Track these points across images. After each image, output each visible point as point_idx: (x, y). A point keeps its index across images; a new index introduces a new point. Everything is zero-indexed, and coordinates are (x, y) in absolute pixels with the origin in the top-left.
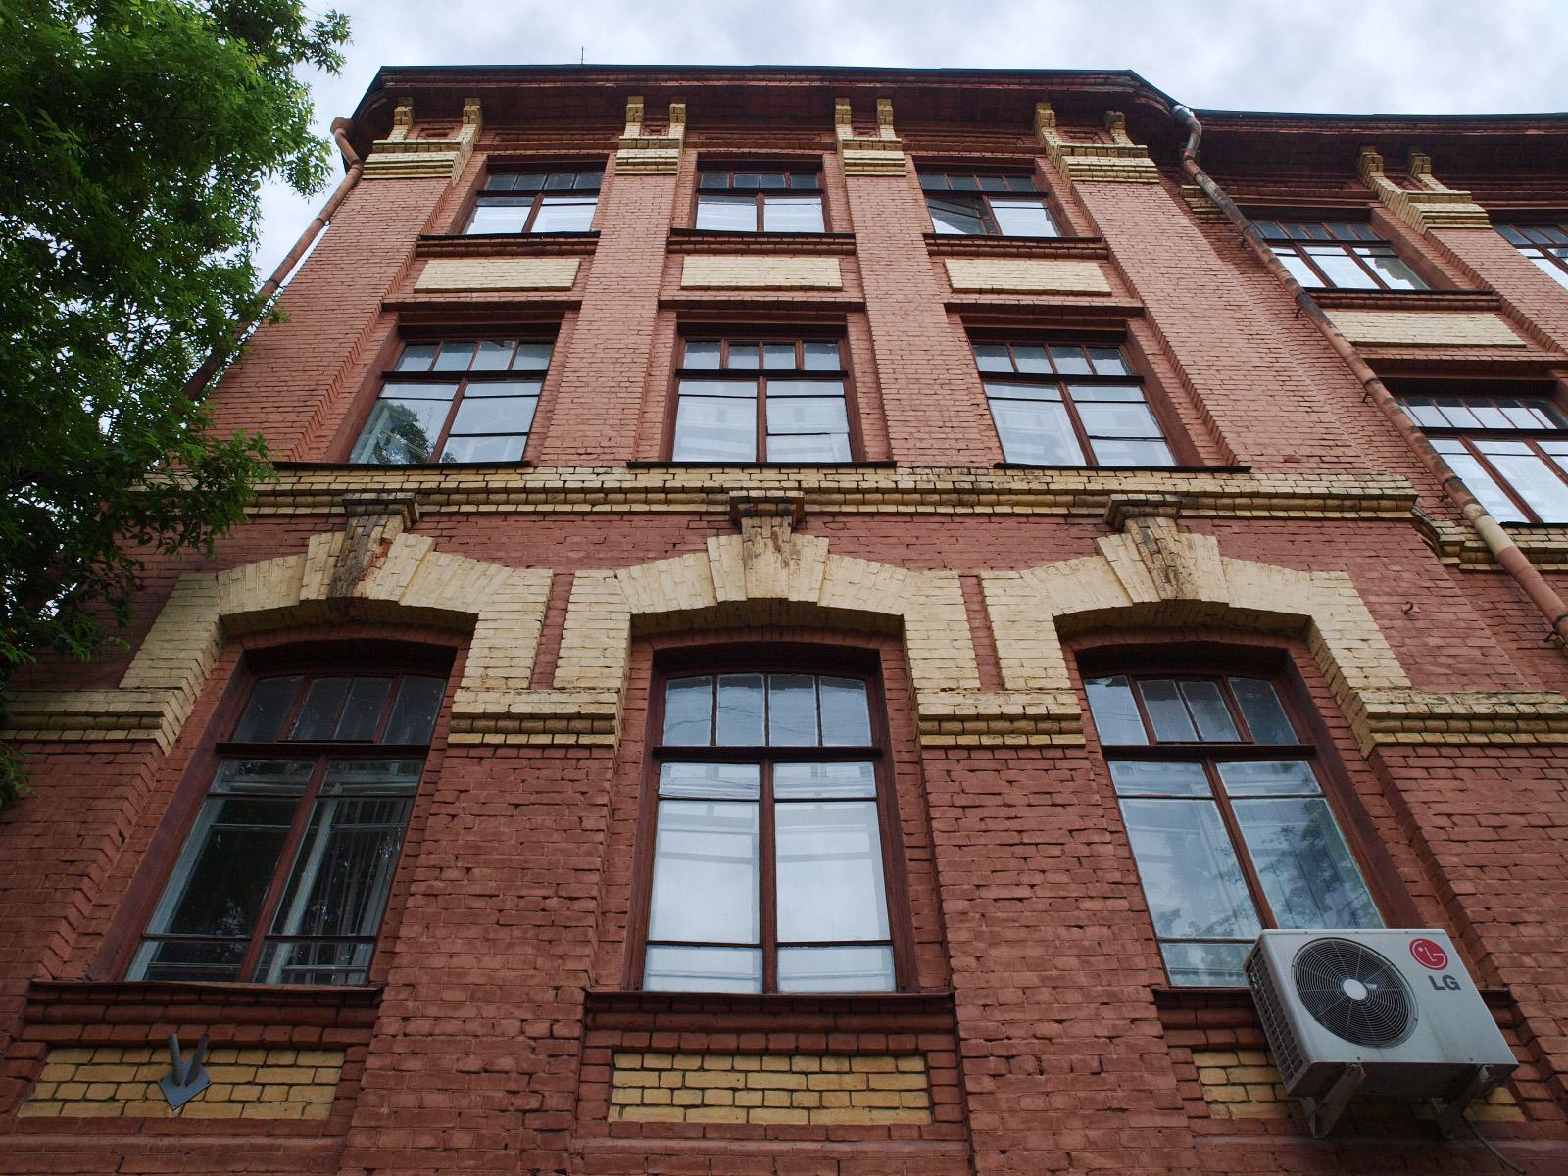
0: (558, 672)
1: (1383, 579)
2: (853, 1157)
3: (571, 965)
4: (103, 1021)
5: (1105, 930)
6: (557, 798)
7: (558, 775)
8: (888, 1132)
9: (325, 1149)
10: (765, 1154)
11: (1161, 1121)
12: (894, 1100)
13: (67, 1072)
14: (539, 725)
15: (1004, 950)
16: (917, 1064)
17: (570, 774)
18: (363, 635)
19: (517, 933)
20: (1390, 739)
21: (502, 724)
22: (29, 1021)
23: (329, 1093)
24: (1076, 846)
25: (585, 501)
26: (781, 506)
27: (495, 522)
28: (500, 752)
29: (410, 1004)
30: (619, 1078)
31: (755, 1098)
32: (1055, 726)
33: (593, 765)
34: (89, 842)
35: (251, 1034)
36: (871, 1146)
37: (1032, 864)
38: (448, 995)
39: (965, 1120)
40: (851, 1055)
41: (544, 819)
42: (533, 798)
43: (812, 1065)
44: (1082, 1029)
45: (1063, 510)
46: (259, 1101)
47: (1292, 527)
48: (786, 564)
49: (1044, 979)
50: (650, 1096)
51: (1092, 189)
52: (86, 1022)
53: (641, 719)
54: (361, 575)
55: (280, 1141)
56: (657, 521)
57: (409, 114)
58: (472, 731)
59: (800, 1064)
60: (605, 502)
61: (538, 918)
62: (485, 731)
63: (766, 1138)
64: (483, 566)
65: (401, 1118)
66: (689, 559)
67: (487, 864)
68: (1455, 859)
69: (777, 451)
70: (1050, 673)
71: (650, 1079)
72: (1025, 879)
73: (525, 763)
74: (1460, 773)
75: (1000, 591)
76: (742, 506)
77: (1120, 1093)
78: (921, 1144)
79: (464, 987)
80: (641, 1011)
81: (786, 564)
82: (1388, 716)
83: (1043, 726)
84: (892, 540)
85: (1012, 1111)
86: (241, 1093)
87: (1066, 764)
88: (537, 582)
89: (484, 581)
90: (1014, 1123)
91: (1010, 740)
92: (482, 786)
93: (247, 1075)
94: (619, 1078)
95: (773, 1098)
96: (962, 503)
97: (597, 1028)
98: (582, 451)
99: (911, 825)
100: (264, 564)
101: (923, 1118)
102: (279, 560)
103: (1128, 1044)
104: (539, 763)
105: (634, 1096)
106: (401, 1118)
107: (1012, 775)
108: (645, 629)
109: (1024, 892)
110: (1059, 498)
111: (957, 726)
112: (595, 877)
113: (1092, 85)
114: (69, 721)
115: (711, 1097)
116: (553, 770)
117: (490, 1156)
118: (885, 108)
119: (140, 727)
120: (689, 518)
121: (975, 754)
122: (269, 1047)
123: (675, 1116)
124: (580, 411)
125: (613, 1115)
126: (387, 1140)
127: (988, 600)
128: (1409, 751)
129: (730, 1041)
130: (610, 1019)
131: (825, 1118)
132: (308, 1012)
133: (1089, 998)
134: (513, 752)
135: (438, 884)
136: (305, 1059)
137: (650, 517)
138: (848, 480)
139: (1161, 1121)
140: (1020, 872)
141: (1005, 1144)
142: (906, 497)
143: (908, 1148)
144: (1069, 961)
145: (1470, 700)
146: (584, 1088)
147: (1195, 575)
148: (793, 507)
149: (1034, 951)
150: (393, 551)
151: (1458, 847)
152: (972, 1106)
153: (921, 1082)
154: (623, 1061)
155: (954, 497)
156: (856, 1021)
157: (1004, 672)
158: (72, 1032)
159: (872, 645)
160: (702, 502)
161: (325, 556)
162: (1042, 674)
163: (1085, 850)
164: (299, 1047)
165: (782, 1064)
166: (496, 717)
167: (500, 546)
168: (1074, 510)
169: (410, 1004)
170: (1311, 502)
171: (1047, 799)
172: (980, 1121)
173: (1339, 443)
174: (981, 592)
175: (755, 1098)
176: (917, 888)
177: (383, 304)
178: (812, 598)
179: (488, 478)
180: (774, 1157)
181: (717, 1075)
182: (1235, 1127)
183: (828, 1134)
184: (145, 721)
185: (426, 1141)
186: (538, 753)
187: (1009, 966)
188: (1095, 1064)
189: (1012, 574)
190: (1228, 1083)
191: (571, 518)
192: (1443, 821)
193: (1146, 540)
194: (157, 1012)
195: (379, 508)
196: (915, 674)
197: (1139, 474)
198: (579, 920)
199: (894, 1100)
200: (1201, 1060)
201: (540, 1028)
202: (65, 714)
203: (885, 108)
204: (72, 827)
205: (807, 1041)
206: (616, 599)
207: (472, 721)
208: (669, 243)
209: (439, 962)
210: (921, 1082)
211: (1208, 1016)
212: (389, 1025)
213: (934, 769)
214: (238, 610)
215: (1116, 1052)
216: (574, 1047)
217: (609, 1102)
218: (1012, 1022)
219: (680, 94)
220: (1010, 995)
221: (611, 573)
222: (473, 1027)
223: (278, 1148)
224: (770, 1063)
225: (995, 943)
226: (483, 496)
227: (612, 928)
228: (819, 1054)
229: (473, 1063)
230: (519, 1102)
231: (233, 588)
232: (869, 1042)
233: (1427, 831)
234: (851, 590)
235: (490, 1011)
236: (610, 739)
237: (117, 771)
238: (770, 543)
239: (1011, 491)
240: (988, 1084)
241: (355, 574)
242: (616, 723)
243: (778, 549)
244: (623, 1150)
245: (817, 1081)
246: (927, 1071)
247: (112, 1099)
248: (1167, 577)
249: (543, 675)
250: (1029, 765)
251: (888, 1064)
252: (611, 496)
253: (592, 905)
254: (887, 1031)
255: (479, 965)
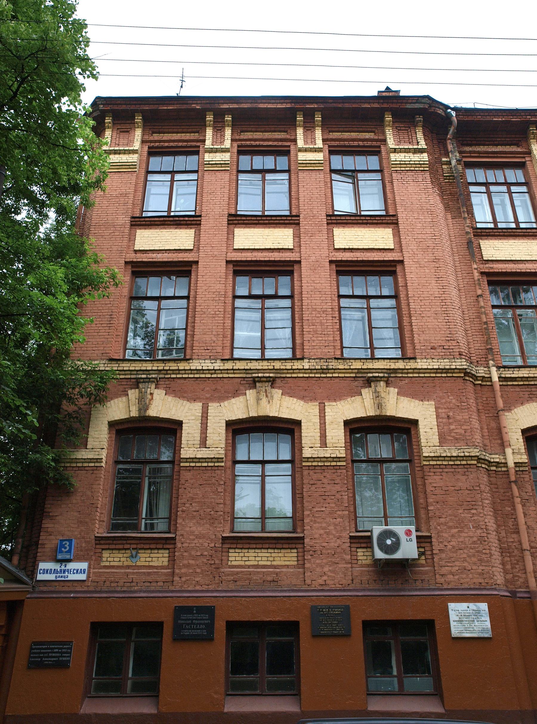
0: (207, 442)
1: (445, 403)
2: (280, 572)
3: (218, 529)
4: (113, 544)
5: (341, 520)
6: (211, 482)
7: (210, 475)
8: (288, 566)
9: (169, 572)
10: (261, 572)
11: (345, 566)
12: (290, 559)
13: (108, 555)
14: (204, 460)
15: (317, 525)
16: (295, 551)
17: (213, 475)
18: (150, 425)
19: (205, 521)
20: (428, 463)
21: (194, 460)
22: (96, 544)
23: (167, 559)
24: (338, 496)
25: (209, 373)
26: (268, 379)
27: (182, 381)
28: (194, 468)
29: (183, 539)
30: (230, 554)
31: (260, 559)
32: (338, 460)
33: (219, 472)
34: (95, 498)
35: (147, 546)
36: (284, 570)
37: (327, 501)
38: (191, 537)
39: (304, 564)
40: (281, 549)
41: (208, 489)
42: (204, 483)
43: (272, 551)
44: (332, 544)
45: (354, 375)
46: (152, 561)
47: (424, 380)
48: (269, 402)
49: (326, 532)
50: (237, 559)
51: (399, 176)
52: (109, 544)
53: (230, 453)
54: (147, 408)
55: (159, 571)
56: (231, 381)
57: (112, 123)
58: (186, 462)
59: (270, 551)
60: (215, 373)
61: (209, 517)
62: (190, 462)
63: (262, 568)
64: (181, 401)
65: (185, 566)
66: (241, 398)
67: (195, 502)
68: (432, 500)
69: (269, 354)
70: (340, 441)
71: (237, 554)
72: (324, 506)
73: (202, 471)
74: (443, 474)
75: (330, 411)
76: (256, 379)
77: (338, 559)
78: (295, 570)
79: (194, 535)
80: (234, 539)
81: (269, 402)
82: (429, 457)
83: (335, 460)
84: (301, 388)
85: (314, 563)
86: (148, 559)
87: (339, 471)
88: (198, 406)
89: (182, 408)
90: (314, 566)
91: (326, 464)
92: (191, 479)
93: (148, 555)
94: (230, 554)
95: (264, 559)
96: (323, 373)
97: (224, 543)
98: (206, 348)
99: (298, 483)
100: (116, 400)
101: (296, 563)
102: (120, 399)
103: (342, 548)
104: (205, 472)
105: (233, 559)
106: (185, 566)
107: (325, 474)
108: (229, 424)
109: (323, 509)
110: (353, 371)
111: (312, 460)
112: (222, 506)
113: (410, 103)
114: (78, 461)
115: (250, 558)
116: (208, 474)
117: (205, 573)
118: (318, 118)
119: (97, 462)
120: (240, 379)
121: (316, 468)
122: (151, 549)
123: (242, 563)
124: (204, 327)
125: (229, 563)
126: (183, 571)
127: (326, 414)
128: (432, 467)
129: (254, 546)
130: (228, 541)
131: (274, 563)
132: (159, 541)
133: (335, 537)
134: (198, 468)
135: (184, 508)
136: (160, 551)
137: (229, 379)
138: (289, 365)
139: (345, 566)
140: (323, 503)
141: (311, 570)
142: (306, 371)
143: (292, 570)
144: (332, 528)
145: (453, 451)
146: (223, 557)
147: (388, 405)
148: (272, 379)
149: (324, 525)
150: (155, 396)
151: (434, 497)
152: (306, 562)
153: (296, 555)
154: (231, 551)
155: (321, 371)
156: (282, 542)
157: (327, 441)
158: (107, 546)
159: (293, 427)
160: (244, 373)
161: (134, 399)
162: (337, 442)
163: (340, 497)
164: (158, 549)
165: (266, 551)
166: (193, 458)
167: (185, 392)
168: (358, 375)
169: (183, 539)
170: (432, 371)
171: (333, 482)
172: (307, 566)
173: (452, 339)
174: (325, 409)
175: (260, 559)
176: (299, 505)
177: (125, 262)
178: (276, 415)
179: (178, 365)
180: (264, 572)
181: (251, 553)
182: (362, 566)
183: (275, 567)
184: (98, 460)
185: (191, 571)
186: (204, 468)
187: (318, 529)
188: (333, 553)
189: (334, 404)
190: (364, 555)
191: (205, 379)
192: (433, 489)
193: (376, 391)
194: (125, 542)
195: (147, 380)
196: (303, 442)
197: (380, 361)
198: (219, 517)
199: (290, 559)
200: (358, 550)
201: (213, 545)
202: (76, 459)
203: (318, 118)
204: (89, 493)
205: (271, 546)
206: (221, 415)
207: (187, 460)
208: (228, 220)
209: (188, 529)
210: (296, 555)
211: (361, 541)
212: (179, 545)
213: (305, 473)
214: (113, 419)
215: (339, 550)
216: (220, 549)
217: (228, 560)
218: (317, 543)
219: (229, 111)
220: (317, 536)
221: (218, 404)
222: (197, 545)
223: (159, 572)
224: (263, 551)
225: (315, 522)
226: (178, 372)
227: (226, 517)
228: (274, 549)
229: (199, 554)
230: (210, 562)
231: (109, 410)
232: (285, 546)
233: (428, 491)
234: (287, 411)
235: (201, 541)
236: (223, 464)
237: (210, 586)
238: (264, 394)
239: (338, 369)
240: (309, 557)
241: (145, 407)
242: (224, 459)
243: (267, 396)
244: (232, 571)
245: (273, 555)
246: (297, 552)
247: (120, 561)
248: (378, 407)
249: (203, 443)
250: (330, 471)
251: (289, 551)
252: (217, 372)
253: (222, 513)
254: (289, 544)
255: (198, 530)
